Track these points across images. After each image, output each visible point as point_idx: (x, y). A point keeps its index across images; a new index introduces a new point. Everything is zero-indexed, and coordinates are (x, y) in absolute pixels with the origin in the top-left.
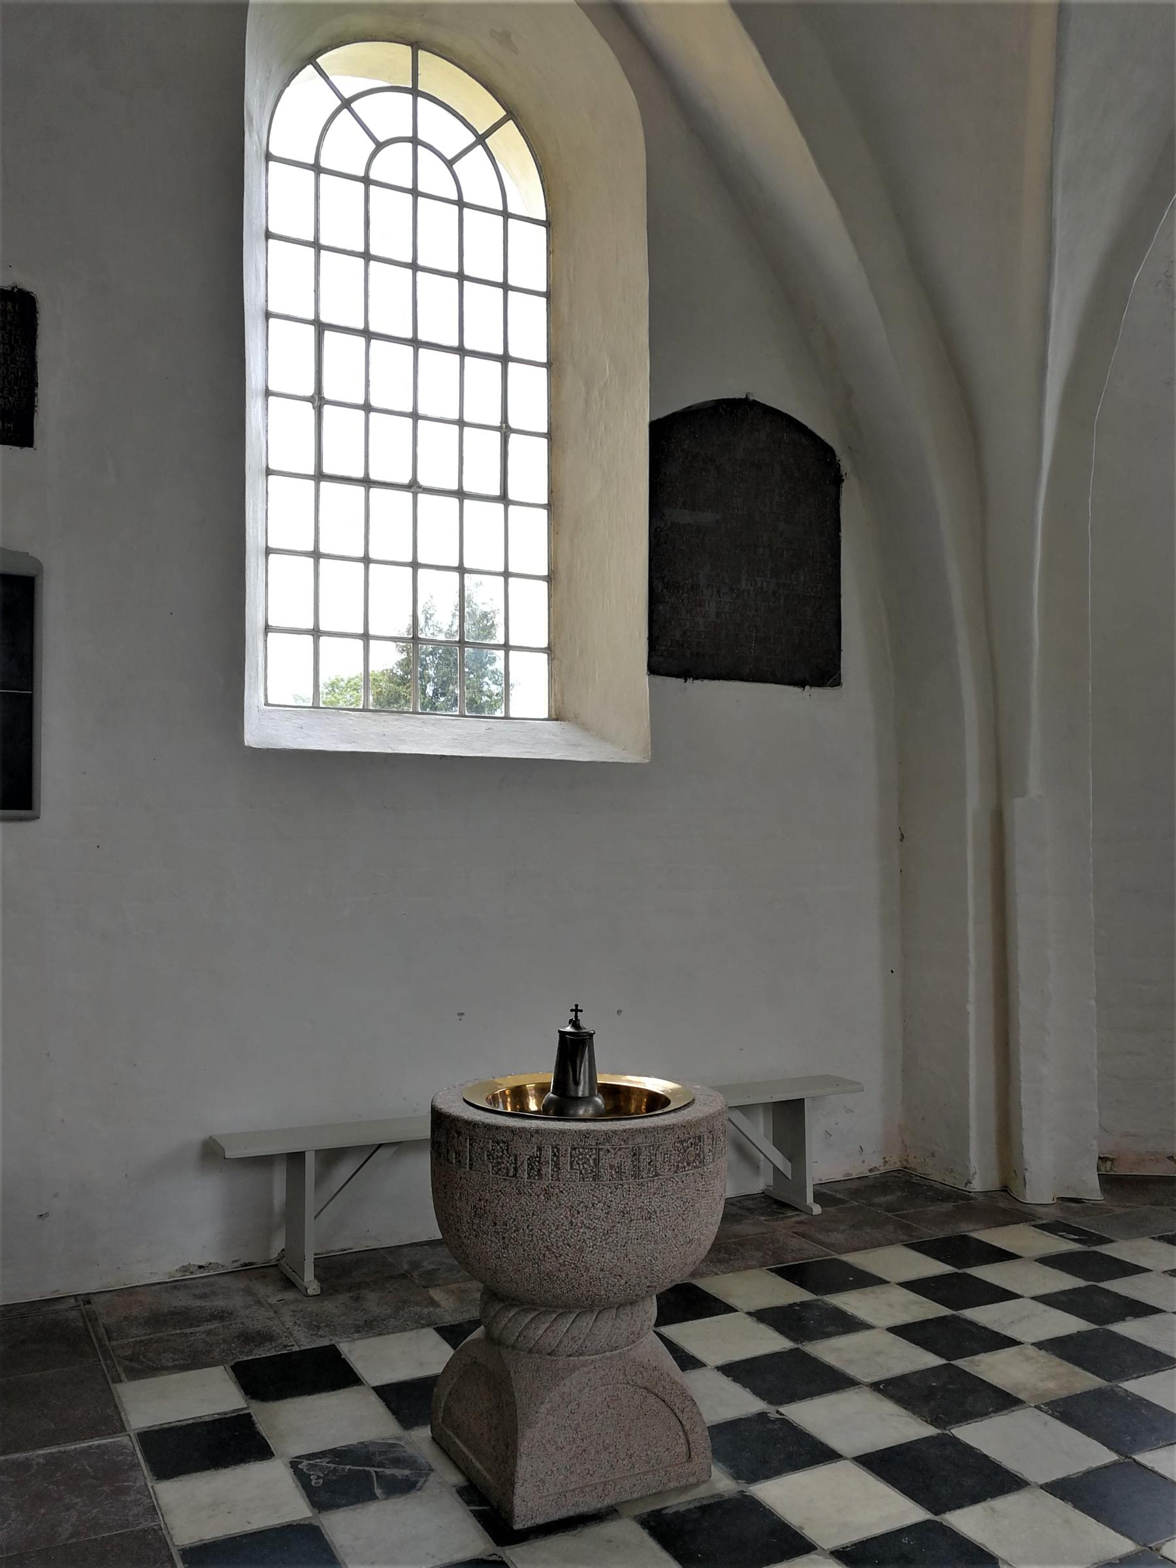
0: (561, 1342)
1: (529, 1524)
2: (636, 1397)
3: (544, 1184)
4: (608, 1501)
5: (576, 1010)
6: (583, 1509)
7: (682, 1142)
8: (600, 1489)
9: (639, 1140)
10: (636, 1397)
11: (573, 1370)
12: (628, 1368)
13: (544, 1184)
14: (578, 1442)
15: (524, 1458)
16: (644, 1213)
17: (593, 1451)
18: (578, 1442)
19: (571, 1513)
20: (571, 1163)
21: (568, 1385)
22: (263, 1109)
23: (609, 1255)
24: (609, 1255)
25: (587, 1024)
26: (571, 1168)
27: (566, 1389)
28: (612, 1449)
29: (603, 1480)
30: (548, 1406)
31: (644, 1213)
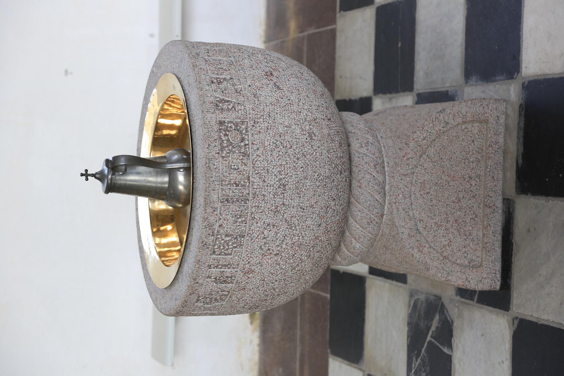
0: (370, 233)
1: (499, 276)
2: (426, 165)
3: (239, 275)
4: (499, 203)
5: (86, 175)
6: (499, 228)
7: (222, 149)
8: (488, 210)
9: (215, 197)
10: (426, 165)
11: (393, 224)
12: (402, 171)
13: (239, 275)
14: (449, 225)
15: (450, 278)
16: (280, 191)
17: (458, 213)
18: (449, 225)
19: (500, 238)
20: (226, 254)
21: (403, 230)
22: (134, 309)
23: (309, 222)
24: (309, 222)
25: (98, 166)
26: (230, 254)
27: (406, 232)
28: (461, 196)
29: (481, 206)
30: (416, 251)
31: (280, 191)
